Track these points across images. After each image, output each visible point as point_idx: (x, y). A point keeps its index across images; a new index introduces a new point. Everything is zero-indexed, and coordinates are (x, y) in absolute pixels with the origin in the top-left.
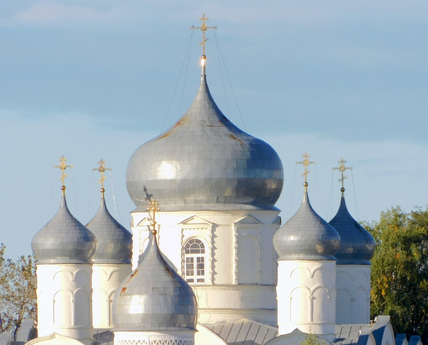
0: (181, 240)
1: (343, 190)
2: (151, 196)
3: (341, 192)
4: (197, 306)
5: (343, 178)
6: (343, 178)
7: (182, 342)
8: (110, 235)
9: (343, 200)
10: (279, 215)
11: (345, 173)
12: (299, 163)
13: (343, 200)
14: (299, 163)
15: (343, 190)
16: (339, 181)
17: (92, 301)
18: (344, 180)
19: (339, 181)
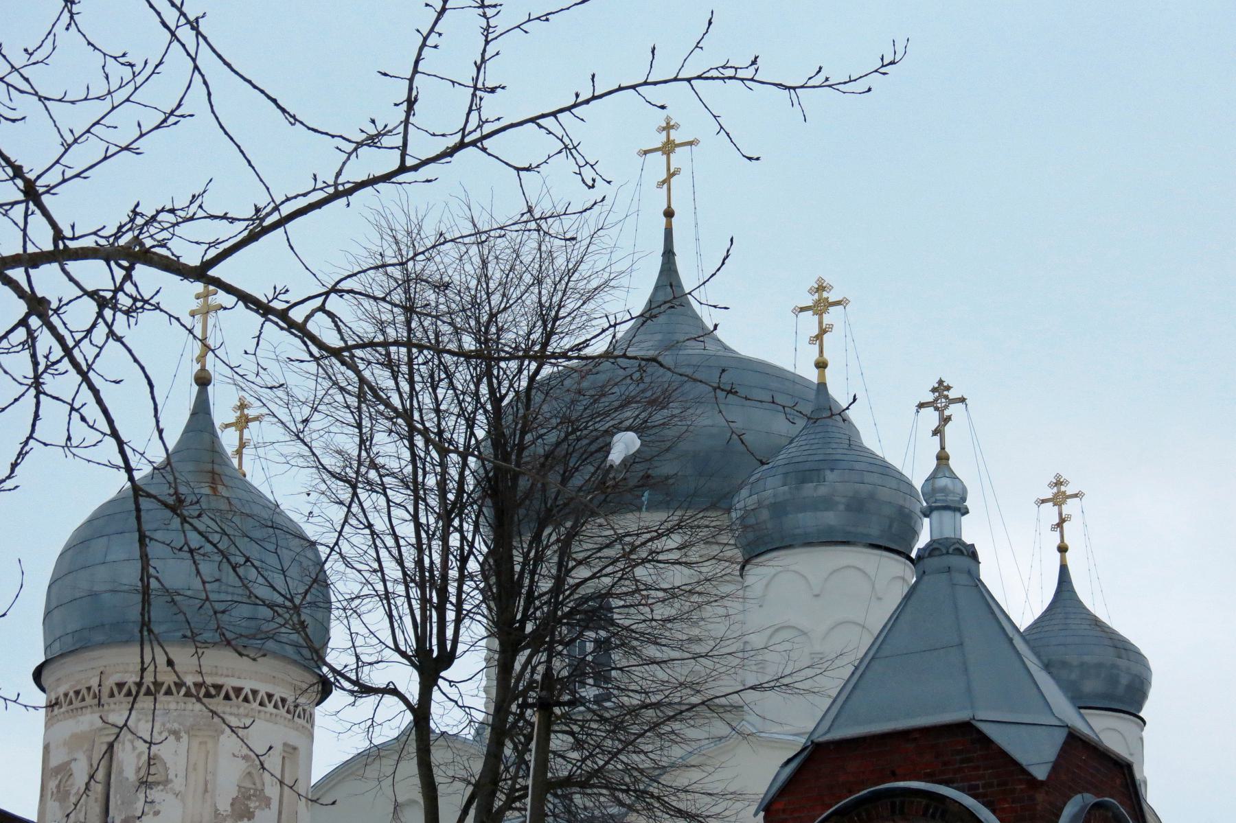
0: (7, 288)
1: (1063, 549)
2: (941, 382)
3: (1058, 554)
4: (1011, 640)
5: (1062, 521)
6: (1062, 521)
7: (275, 698)
8: (840, 414)
9: (1064, 570)
10: (86, 387)
11: (1066, 509)
12: (802, 309)
13: (1064, 570)
14: (802, 309)
15: (1063, 549)
16: (1053, 528)
17: (973, 545)
18: (1065, 525)
19: (1053, 528)
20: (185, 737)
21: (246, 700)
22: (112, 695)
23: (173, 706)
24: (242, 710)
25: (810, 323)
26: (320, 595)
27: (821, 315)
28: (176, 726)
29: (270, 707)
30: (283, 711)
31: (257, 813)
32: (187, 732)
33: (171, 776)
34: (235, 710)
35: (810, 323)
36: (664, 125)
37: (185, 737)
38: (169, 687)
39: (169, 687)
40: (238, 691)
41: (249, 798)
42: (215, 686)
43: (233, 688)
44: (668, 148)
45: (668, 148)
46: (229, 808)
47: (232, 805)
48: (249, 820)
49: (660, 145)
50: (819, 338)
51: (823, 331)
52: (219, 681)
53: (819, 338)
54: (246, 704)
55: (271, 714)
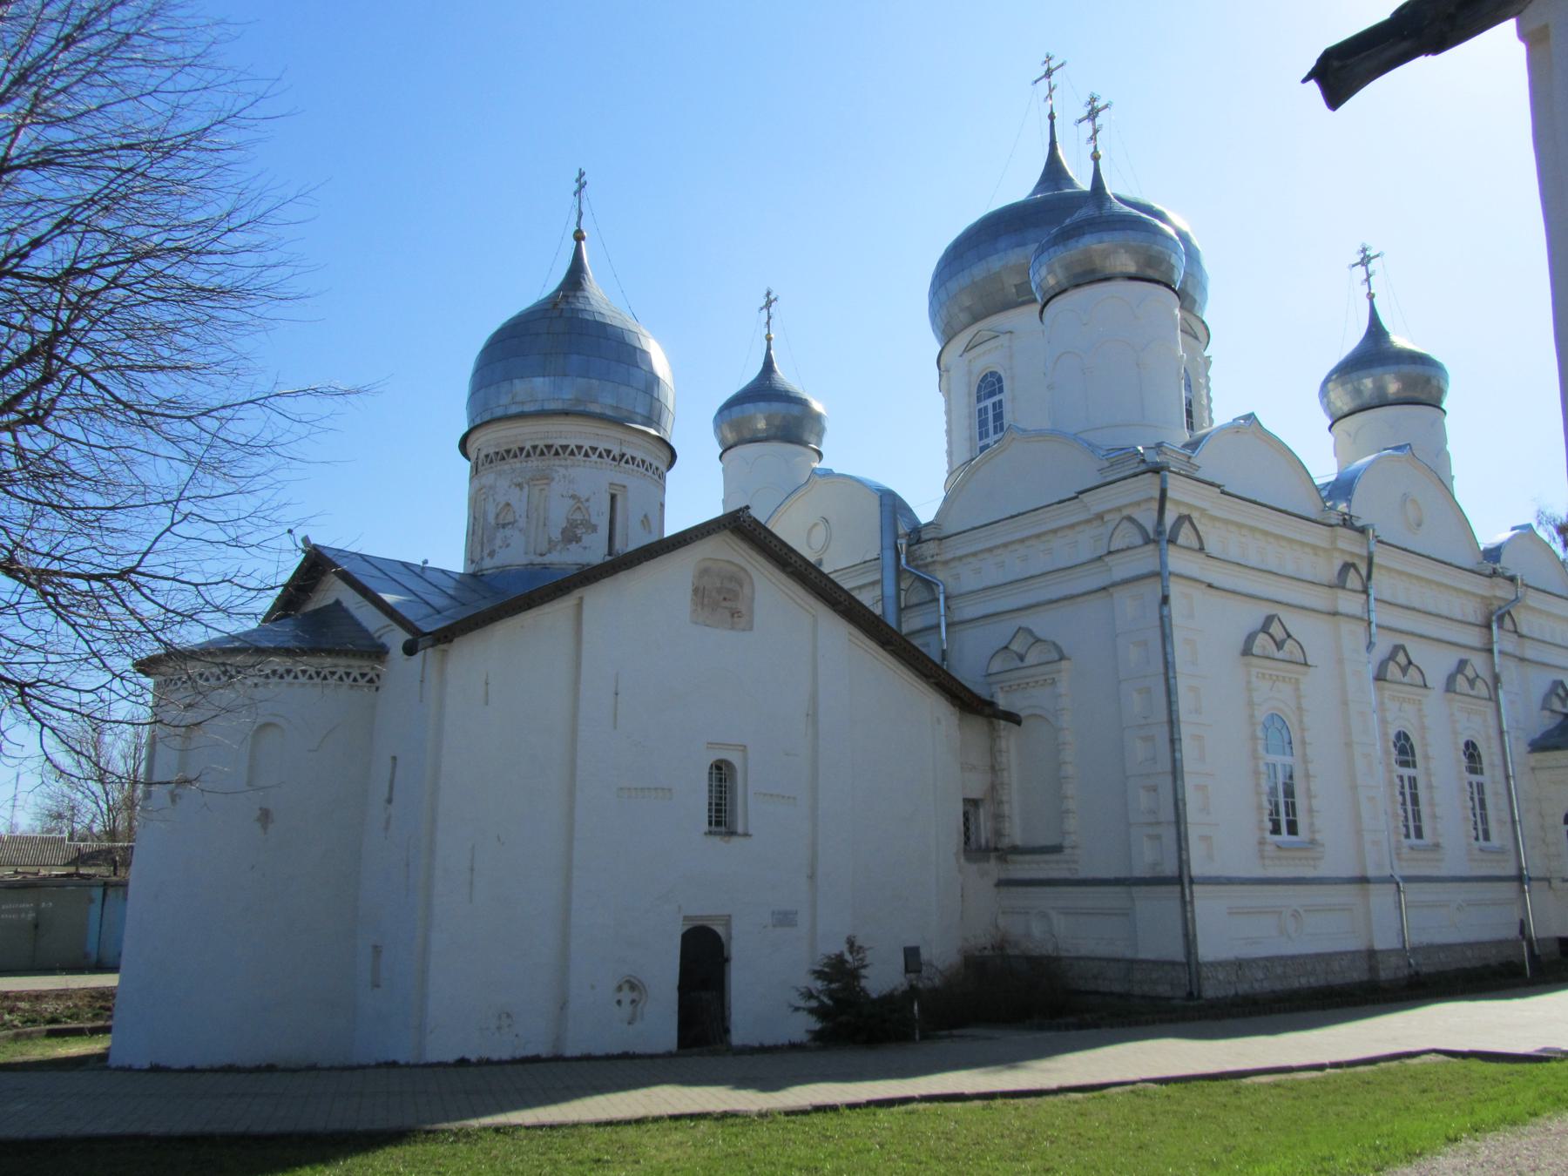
11: (1371, 267)
20: (526, 486)
21: (572, 453)
22: (483, 465)
23: (518, 465)
24: (569, 462)
25: (1361, 270)
26: (150, 353)
27: (1366, 266)
28: (520, 480)
29: (594, 458)
30: (609, 461)
31: (584, 537)
32: (528, 483)
33: (517, 517)
34: (563, 463)
35: (1087, 127)
36: (1045, 59)
37: (526, 486)
38: (572, 450)
39: (572, 450)
40: (564, 448)
41: (576, 527)
42: (592, 448)
43: (561, 446)
44: (1049, 73)
45: (1049, 73)
46: (560, 537)
47: (562, 533)
48: (577, 542)
49: (1373, 261)
50: (1093, 138)
51: (1096, 131)
52: (549, 442)
53: (1093, 138)
54: (572, 457)
55: (596, 462)
